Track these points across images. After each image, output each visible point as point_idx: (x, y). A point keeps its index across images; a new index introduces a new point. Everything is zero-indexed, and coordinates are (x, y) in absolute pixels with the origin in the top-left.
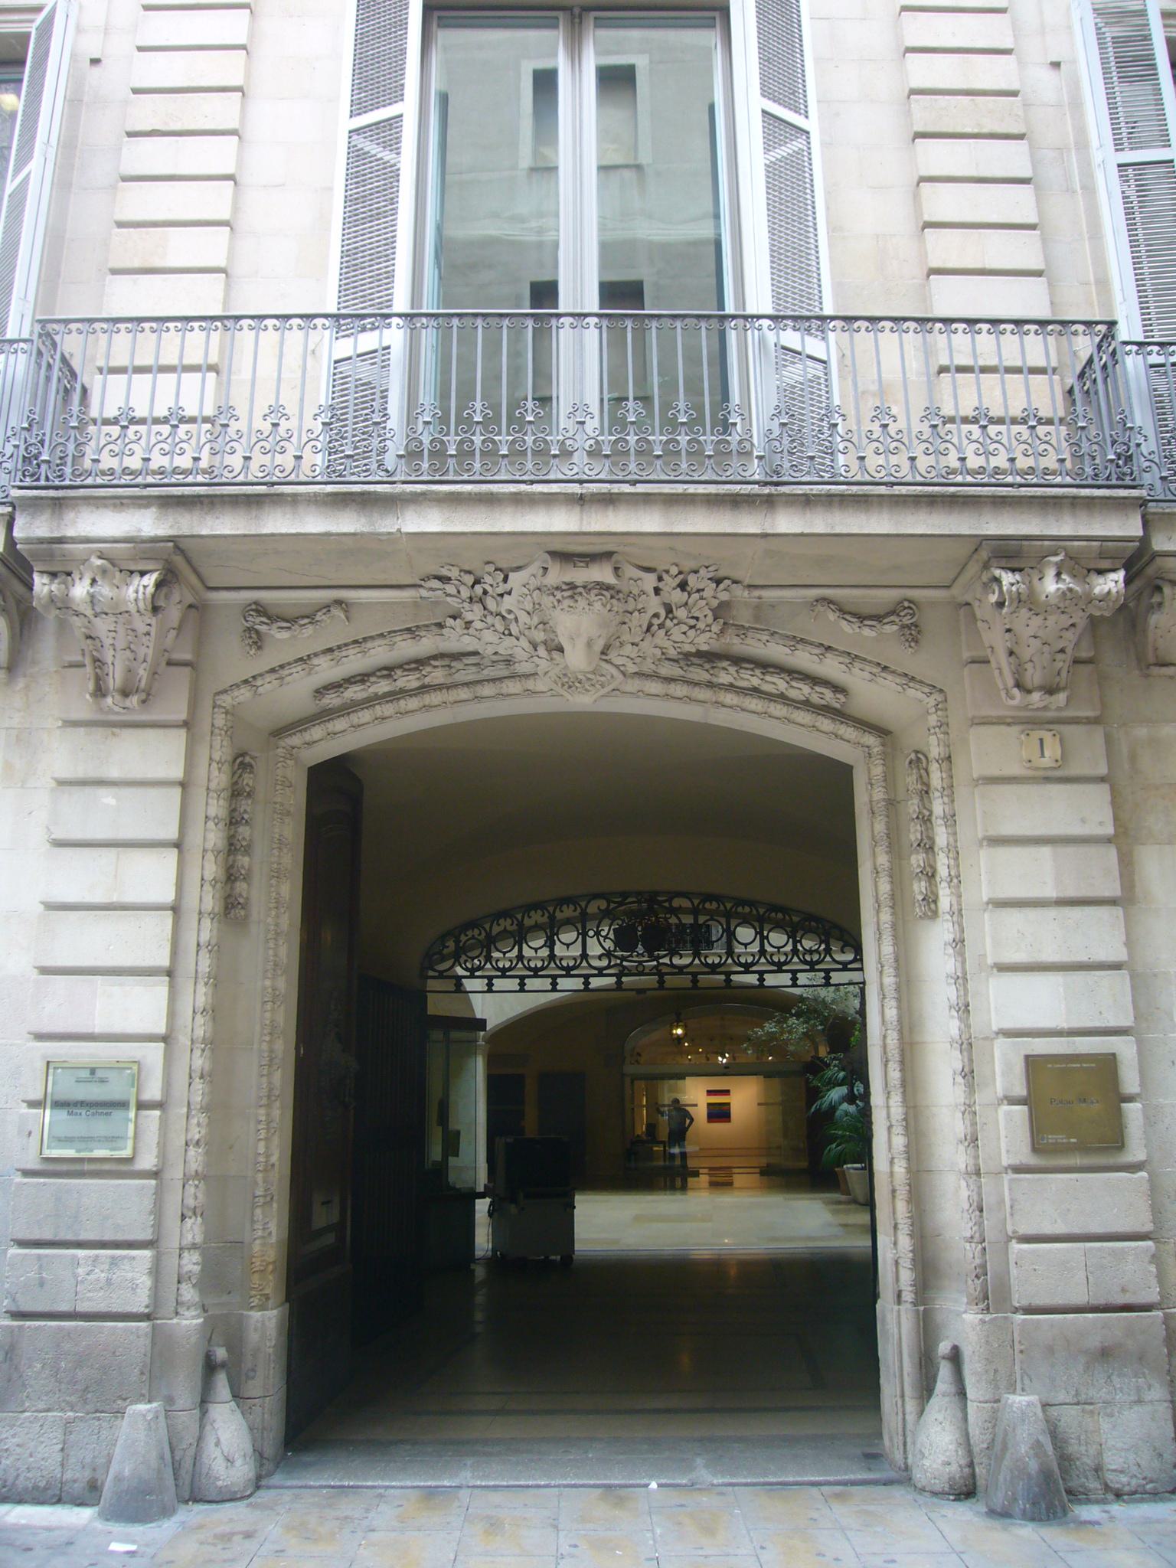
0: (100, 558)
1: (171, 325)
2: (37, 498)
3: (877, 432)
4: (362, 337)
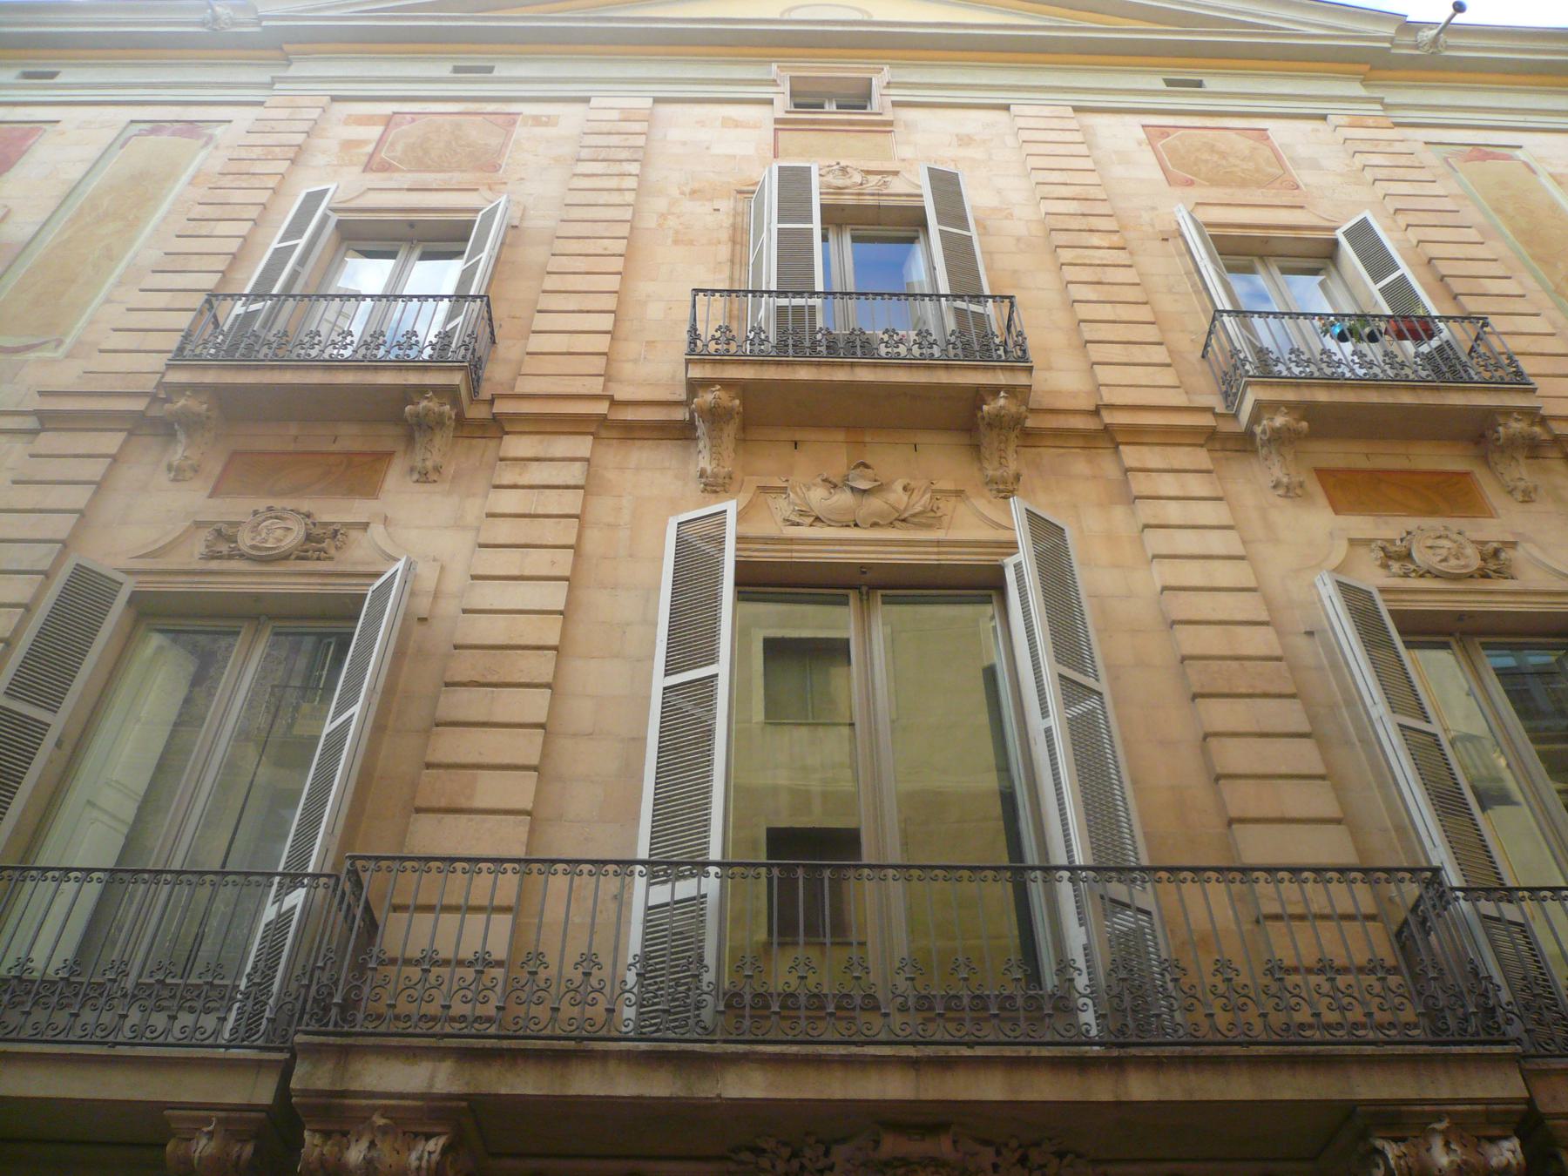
0: (383, 1116)
1: (483, 865)
2: (322, 1044)
3: (1222, 988)
4: (680, 885)
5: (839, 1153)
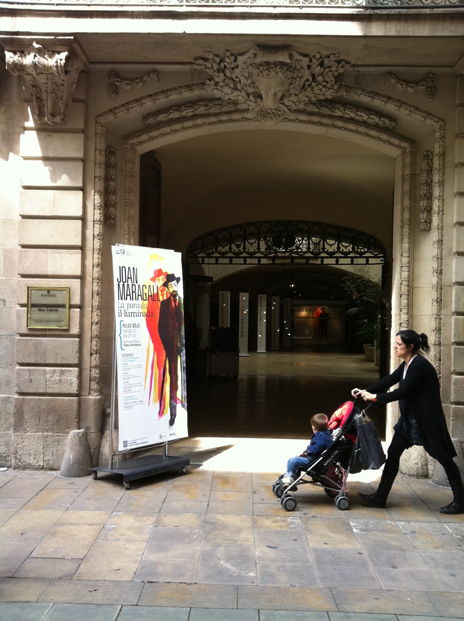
5: (241, 59)
